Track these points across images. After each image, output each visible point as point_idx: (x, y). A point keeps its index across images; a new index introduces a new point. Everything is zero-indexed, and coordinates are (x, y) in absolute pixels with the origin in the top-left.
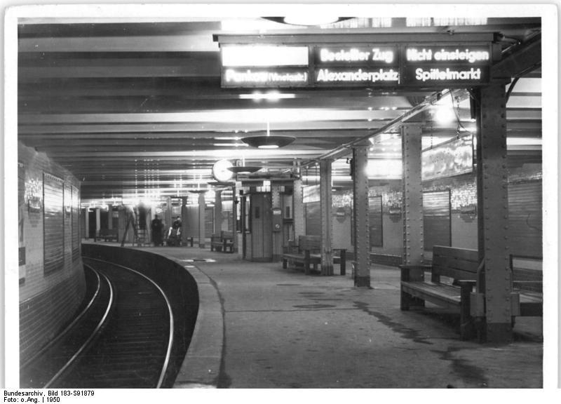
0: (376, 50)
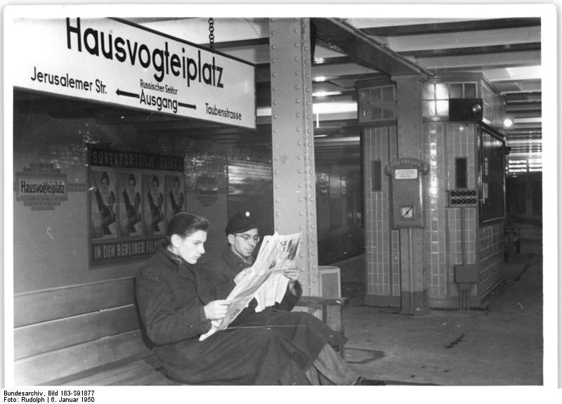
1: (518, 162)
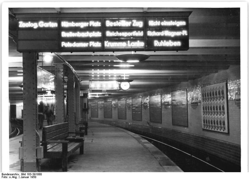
0: (134, 21)
1: (83, 25)
